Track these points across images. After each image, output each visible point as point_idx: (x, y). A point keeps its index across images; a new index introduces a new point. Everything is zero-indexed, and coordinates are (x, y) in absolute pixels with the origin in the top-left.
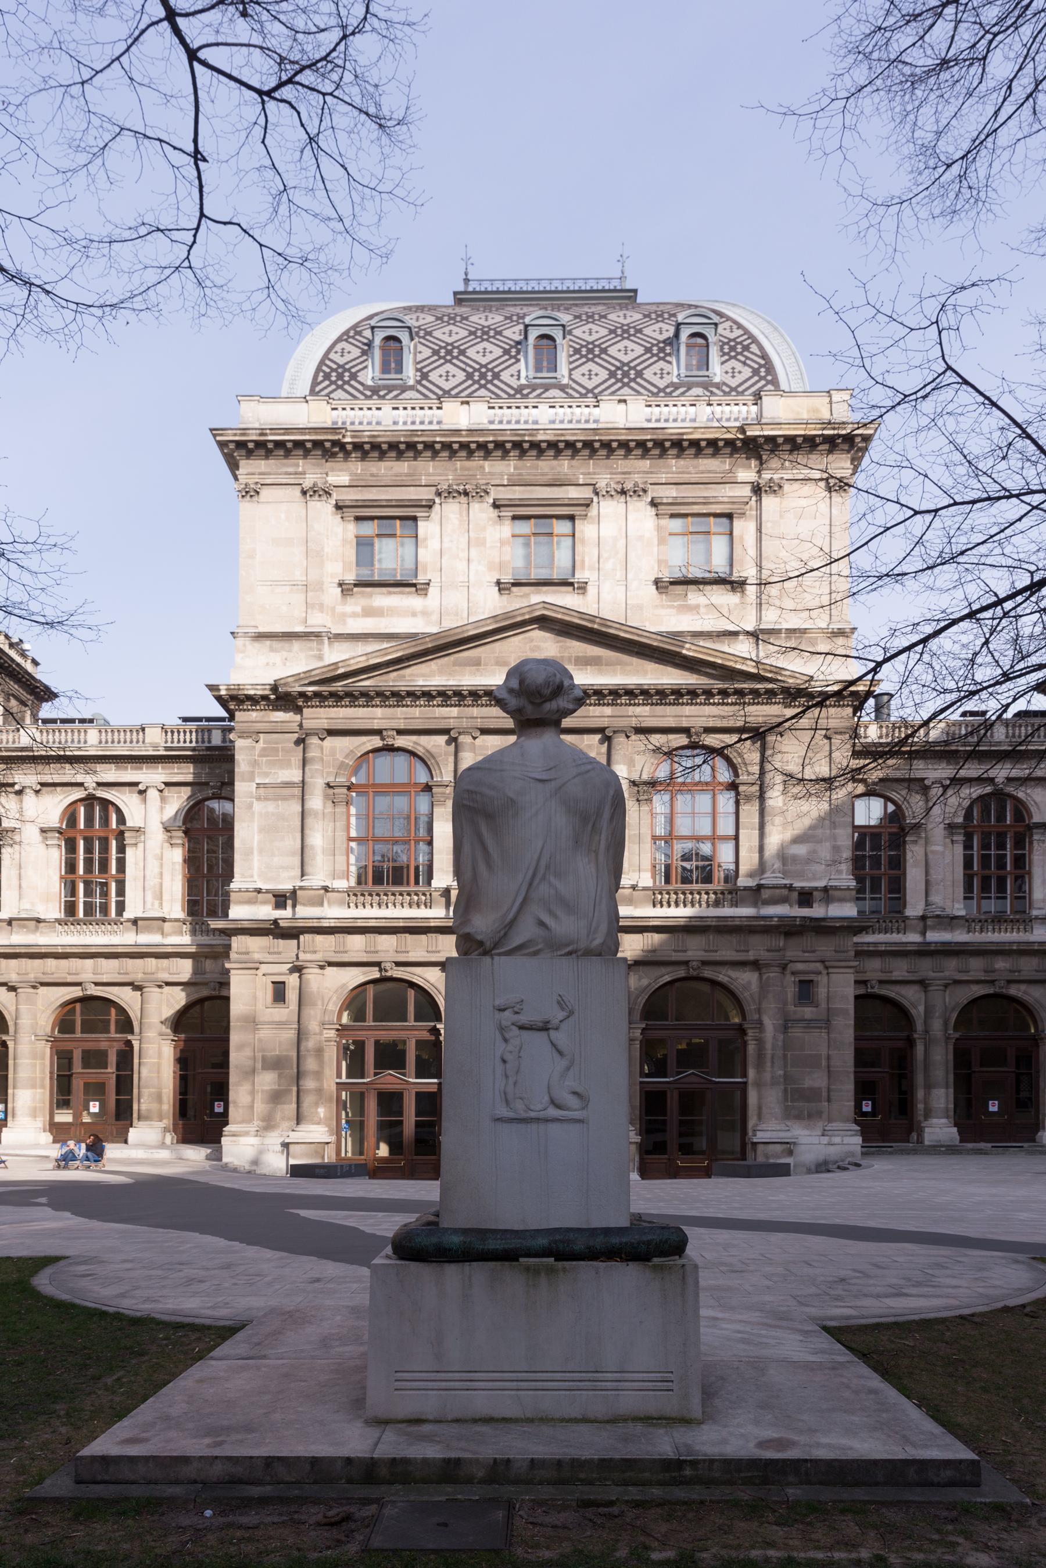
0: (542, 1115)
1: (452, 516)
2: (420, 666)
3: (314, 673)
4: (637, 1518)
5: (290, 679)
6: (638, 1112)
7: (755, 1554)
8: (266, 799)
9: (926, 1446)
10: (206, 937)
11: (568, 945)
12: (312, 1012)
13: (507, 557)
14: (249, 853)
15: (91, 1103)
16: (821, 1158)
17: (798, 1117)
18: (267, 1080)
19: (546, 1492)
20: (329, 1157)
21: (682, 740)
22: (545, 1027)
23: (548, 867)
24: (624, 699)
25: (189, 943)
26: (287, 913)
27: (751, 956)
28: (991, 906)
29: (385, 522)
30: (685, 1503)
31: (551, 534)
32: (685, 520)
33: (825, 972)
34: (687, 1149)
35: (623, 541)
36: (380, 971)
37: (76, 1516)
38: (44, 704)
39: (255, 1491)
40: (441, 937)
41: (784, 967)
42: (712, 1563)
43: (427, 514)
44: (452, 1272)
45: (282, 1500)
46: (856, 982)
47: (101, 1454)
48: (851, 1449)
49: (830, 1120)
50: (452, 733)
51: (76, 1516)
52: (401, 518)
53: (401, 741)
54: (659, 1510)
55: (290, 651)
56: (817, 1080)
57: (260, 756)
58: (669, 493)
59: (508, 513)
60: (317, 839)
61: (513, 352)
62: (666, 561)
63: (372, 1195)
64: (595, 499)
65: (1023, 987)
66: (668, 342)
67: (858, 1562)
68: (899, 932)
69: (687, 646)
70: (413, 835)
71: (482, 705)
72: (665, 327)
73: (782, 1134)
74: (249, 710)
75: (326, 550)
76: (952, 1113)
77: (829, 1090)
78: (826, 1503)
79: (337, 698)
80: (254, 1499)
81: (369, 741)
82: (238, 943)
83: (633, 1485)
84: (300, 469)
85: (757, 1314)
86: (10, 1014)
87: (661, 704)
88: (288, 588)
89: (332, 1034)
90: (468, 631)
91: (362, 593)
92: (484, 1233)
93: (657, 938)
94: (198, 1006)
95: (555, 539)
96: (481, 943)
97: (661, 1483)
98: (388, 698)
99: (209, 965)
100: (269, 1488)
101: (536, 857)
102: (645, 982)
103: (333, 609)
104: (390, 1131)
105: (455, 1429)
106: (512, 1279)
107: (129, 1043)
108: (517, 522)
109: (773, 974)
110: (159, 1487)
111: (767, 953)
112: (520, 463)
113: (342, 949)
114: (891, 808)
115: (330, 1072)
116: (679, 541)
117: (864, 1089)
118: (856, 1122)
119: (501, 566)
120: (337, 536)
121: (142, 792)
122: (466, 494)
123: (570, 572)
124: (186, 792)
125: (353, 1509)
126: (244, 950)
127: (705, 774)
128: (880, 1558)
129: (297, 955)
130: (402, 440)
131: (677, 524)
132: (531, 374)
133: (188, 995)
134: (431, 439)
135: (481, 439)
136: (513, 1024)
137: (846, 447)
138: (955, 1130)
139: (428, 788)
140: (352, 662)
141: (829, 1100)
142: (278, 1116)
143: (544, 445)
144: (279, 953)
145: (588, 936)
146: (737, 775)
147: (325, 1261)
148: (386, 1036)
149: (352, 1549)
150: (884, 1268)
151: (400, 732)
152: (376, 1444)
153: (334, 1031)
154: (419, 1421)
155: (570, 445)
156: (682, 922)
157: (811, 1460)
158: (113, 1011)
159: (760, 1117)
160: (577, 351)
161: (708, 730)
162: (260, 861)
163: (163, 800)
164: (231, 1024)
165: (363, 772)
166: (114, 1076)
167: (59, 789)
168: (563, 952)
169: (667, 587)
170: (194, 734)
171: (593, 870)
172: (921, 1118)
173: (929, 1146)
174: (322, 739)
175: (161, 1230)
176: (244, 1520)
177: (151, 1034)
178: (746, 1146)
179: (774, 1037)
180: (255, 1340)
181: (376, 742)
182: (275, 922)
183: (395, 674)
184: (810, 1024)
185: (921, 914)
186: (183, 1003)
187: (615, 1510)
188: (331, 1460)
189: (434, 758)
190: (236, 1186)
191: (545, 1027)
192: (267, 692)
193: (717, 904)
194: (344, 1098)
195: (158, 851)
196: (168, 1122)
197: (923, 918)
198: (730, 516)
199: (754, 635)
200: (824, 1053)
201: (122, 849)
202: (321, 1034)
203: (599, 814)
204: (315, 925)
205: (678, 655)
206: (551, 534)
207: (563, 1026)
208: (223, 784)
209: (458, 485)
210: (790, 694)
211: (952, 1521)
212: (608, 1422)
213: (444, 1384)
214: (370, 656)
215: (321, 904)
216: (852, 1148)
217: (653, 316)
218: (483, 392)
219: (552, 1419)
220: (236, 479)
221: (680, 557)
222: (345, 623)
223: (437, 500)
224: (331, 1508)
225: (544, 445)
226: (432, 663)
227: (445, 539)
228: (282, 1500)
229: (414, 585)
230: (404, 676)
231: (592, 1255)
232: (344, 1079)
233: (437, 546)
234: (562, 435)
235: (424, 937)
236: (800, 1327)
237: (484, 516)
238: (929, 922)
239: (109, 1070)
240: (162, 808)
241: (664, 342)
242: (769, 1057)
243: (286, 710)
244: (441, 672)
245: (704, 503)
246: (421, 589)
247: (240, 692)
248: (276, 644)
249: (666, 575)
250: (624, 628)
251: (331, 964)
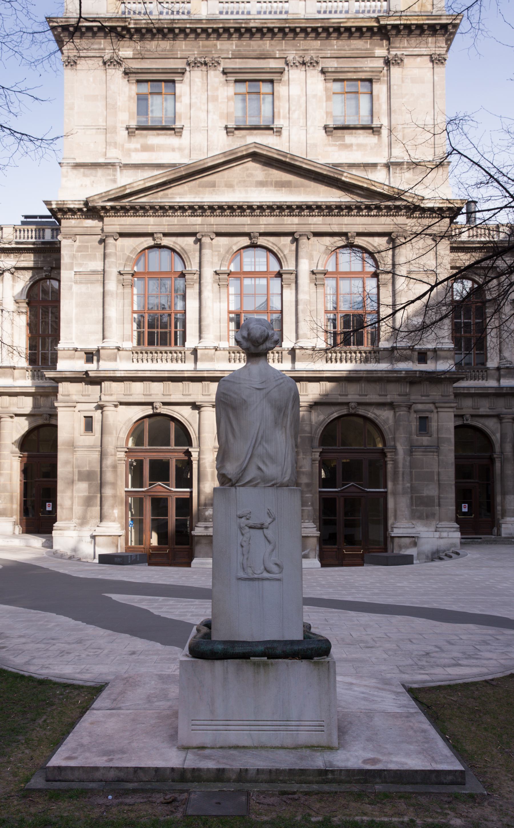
0: (260, 576)
1: (197, 80)
2: (177, 187)
3: (111, 193)
4: (306, 800)
5: (96, 197)
6: (318, 514)
7: (358, 818)
8: (81, 283)
9: (441, 763)
10: (41, 381)
11: (272, 481)
12: (110, 439)
13: (232, 110)
16: (435, 548)
19: (264, 787)
22: (261, 527)
23: (262, 437)
24: (306, 212)
25: (30, 385)
27: (388, 399)
29: (155, 83)
30: (328, 793)
31: (258, 93)
32: (343, 83)
33: (435, 411)
34: (350, 540)
35: (304, 98)
36: (153, 409)
37: (50, 798)
39: (130, 786)
41: (409, 407)
42: (338, 823)
43: (181, 79)
44: (218, 664)
45: (143, 791)
46: (455, 416)
47: (57, 765)
48: (406, 764)
49: (440, 520)
50: (198, 235)
51: (50, 798)
52: (165, 81)
53: (166, 241)
54: (316, 797)
55: (96, 176)
56: (431, 491)
57: (77, 251)
58: (332, 64)
59: (232, 78)
60: (112, 312)
62: (331, 113)
63: (152, 581)
67: (402, 823)
68: (483, 379)
69: (345, 174)
70: (173, 309)
71: (217, 216)
74: (70, 219)
75: (118, 104)
77: (439, 498)
78: (393, 793)
80: (130, 790)
81: (145, 241)
82: (63, 387)
83: (305, 783)
84: (102, 46)
85: (374, 681)
87: (329, 216)
88: (94, 131)
89: (122, 455)
90: (207, 163)
91: (141, 134)
93: (328, 386)
94: (36, 432)
95: (262, 96)
96: (230, 480)
97: (317, 782)
98: (157, 210)
99: (42, 401)
100: (136, 784)
101: (256, 432)
102: (322, 418)
103: (123, 146)
104: (160, 528)
105: (221, 752)
106: (246, 669)
108: (238, 84)
109: (402, 412)
110: (85, 783)
111: (399, 397)
112: (239, 43)
113: (128, 393)
114: (476, 286)
115: (121, 483)
116: (339, 98)
117: (462, 495)
119: (228, 116)
120: (124, 92)
122: (206, 64)
123: (271, 119)
124: (28, 275)
125: (176, 795)
126: (66, 393)
127: (357, 266)
128: (412, 821)
129: (100, 397)
130: (166, 26)
131: (337, 87)
133: (30, 424)
134: (183, 26)
135: (215, 26)
137: (443, 32)
139: (182, 275)
140: (135, 185)
141: (439, 505)
142: (89, 515)
143: (254, 30)
144: (89, 395)
145: (282, 475)
146: (377, 267)
147: (135, 638)
149: (179, 815)
150: (453, 644)
151: (165, 235)
152: (185, 760)
153: (123, 453)
154: (203, 748)
155: (270, 30)
156: (344, 374)
157: (387, 770)
159: (395, 518)
162: (76, 330)
164: (59, 447)
168: (270, 484)
169: (332, 132)
170: (34, 232)
171: (284, 438)
172: (500, 517)
173: (505, 538)
174: (116, 240)
175: (32, 611)
176: (127, 801)
179: (404, 459)
180: (113, 697)
181: (149, 242)
182: (86, 373)
183: (162, 193)
184: (426, 449)
185: (496, 366)
186: (26, 429)
187: (296, 796)
188: (165, 769)
189: (186, 253)
190: (66, 572)
191: (261, 527)
192: (82, 206)
193: (366, 360)
194: (130, 502)
196: (16, 517)
197: (498, 369)
198: (370, 81)
200: (436, 470)
202: (115, 455)
203: (286, 407)
204: (112, 375)
205: (340, 180)
206: (258, 93)
208: (52, 268)
209: (201, 58)
210: (410, 209)
211: (450, 803)
212: (294, 748)
213: (214, 727)
214: (146, 181)
215: (115, 360)
219: (267, 747)
221: (340, 111)
222: (130, 156)
223: (188, 69)
224: (166, 795)
226: (185, 185)
227: (193, 97)
228: (143, 791)
229: (173, 129)
230: (167, 195)
231: (285, 656)
232: (130, 489)
233: (188, 102)
234: (265, 23)
235: (180, 384)
236: (395, 690)
237: (217, 80)
238: (502, 372)
240: (13, 286)
243: (93, 218)
245: (355, 72)
246: (178, 132)
247: (65, 206)
248: (87, 171)
249: (331, 124)
250: (305, 161)
251: (122, 404)
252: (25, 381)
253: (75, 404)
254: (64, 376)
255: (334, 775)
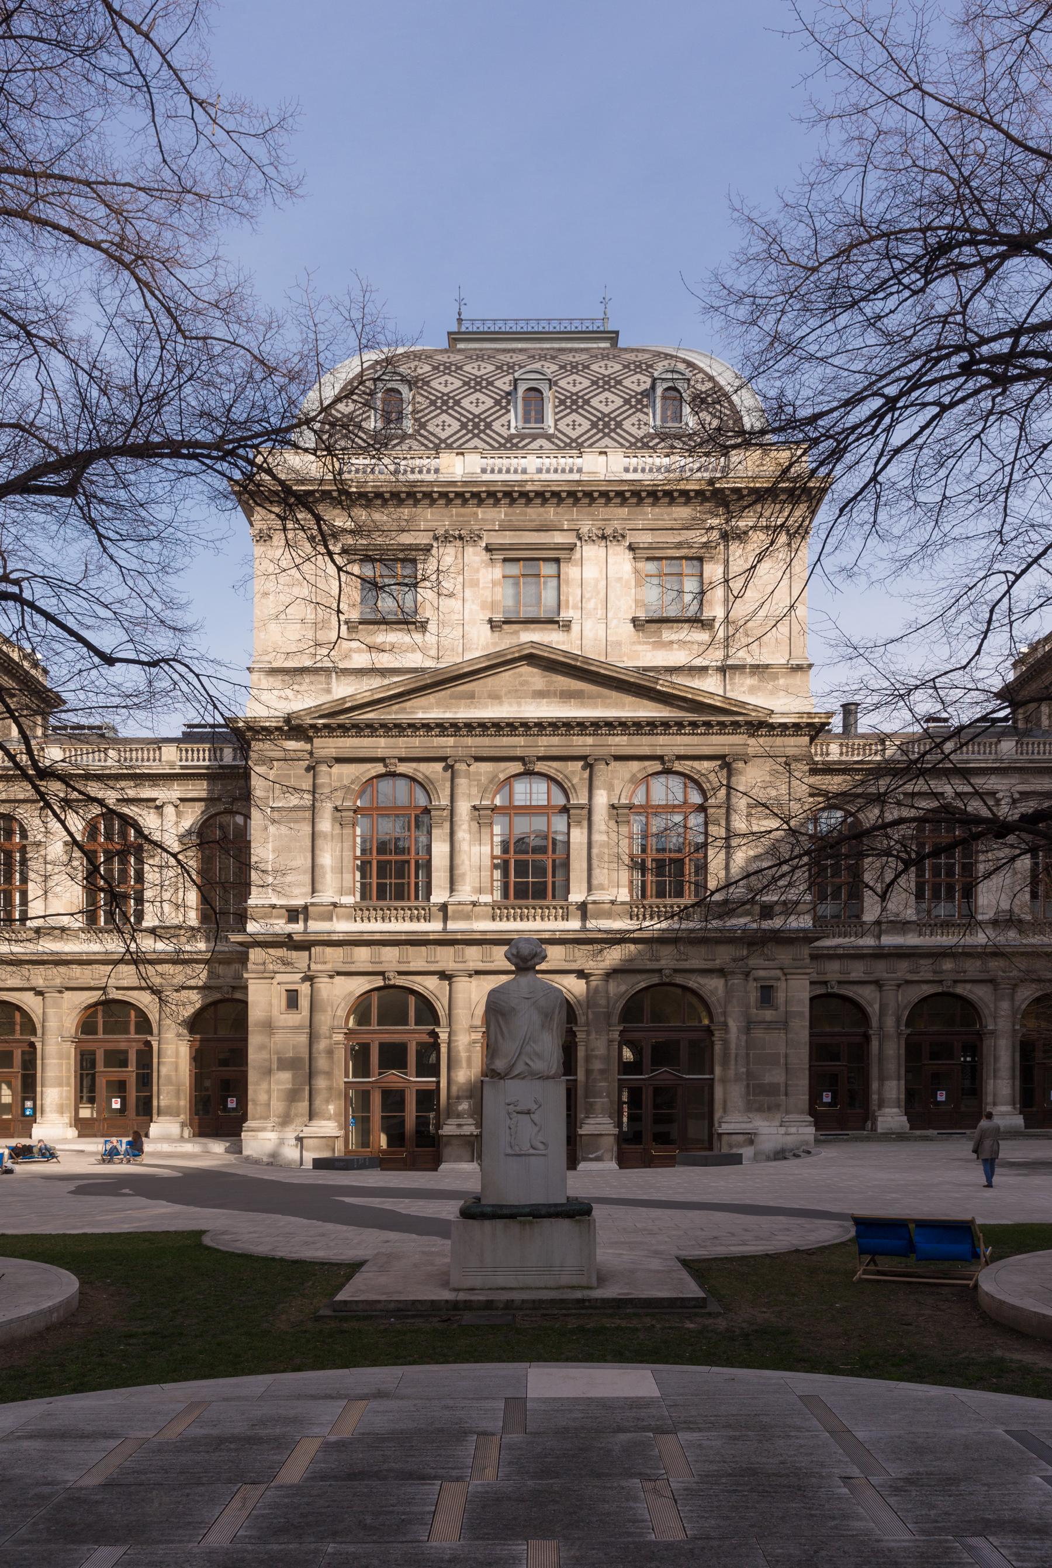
13: (498, 597)
16: (779, 1147)
17: (760, 1110)
18: (283, 1079)
20: (339, 1150)
21: (657, 766)
22: (528, 1112)
26: (299, 927)
28: (942, 910)
34: (663, 1139)
40: (439, 948)
41: (747, 975)
44: (487, 1224)
49: (787, 1113)
53: (402, 768)
56: (775, 1076)
58: (645, 538)
60: (326, 859)
61: (504, 403)
64: (579, 544)
65: (968, 986)
66: (646, 394)
72: (643, 378)
73: (744, 1126)
76: (903, 1104)
79: (344, 730)
82: (255, 955)
89: (340, 1037)
92: (501, 1206)
102: (623, 988)
106: (514, 1227)
107: (148, 1044)
109: (736, 981)
112: (510, 510)
117: (819, 1081)
118: (810, 1115)
119: (493, 605)
122: (461, 538)
124: (199, 807)
131: (651, 567)
132: (520, 425)
138: (905, 1118)
141: (786, 1095)
143: (532, 495)
148: (387, 1038)
151: (402, 760)
155: (555, 494)
158: (133, 1013)
159: (725, 1110)
160: (562, 402)
161: (680, 758)
163: (179, 814)
165: (367, 795)
178: (711, 1139)
179: (738, 1038)
181: (380, 768)
191: (528, 1112)
197: (878, 923)
198: (700, 559)
199: (723, 670)
200: (782, 1051)
202: (331, 1037)
206: (538, 576)
215: (331, 919)
216: (806, 1138)
217: (632, 367)
218: (476, 442)
220: (252, 525)
223: (435, 545)
225: (532, 495)
231: (549, 1216)
232: (351, 1079)
237: (477, 559)
241: (641, 393)
242: (733, 1056)
243: (297, 740)
244: (439, 704)
251: (339, 973)
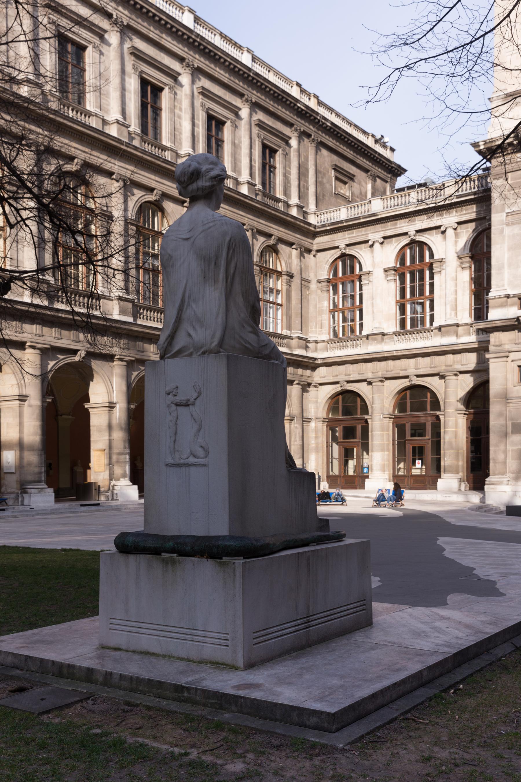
0: (186, 462)
8: (513, 224)
11: (201, 348)
14: (501, 268)
15: (417, 461)
23: (190, 297)
25: (475, 340)
38: (399, 178)
86: (369, 401)
121: (443, 232)
124: (472, 225)
126: (498, 343)
133: (474, 380)
136: (172, 403)
158: (429, 395)
163: (457, 235)
166: (430, 441)
167: (394, 239)
177: (450, 410)
186: (471, 385)
188: (48, 661)
195: (454, 275)
201: (432, 277)
207: (197, 402)
219: (174, 657)
239: (427, 438)
240: (456, 242)
247: (493, 144)
252: (469, 337)
253: (507, 354)
254: (494, 325)
255: (189, 693)
